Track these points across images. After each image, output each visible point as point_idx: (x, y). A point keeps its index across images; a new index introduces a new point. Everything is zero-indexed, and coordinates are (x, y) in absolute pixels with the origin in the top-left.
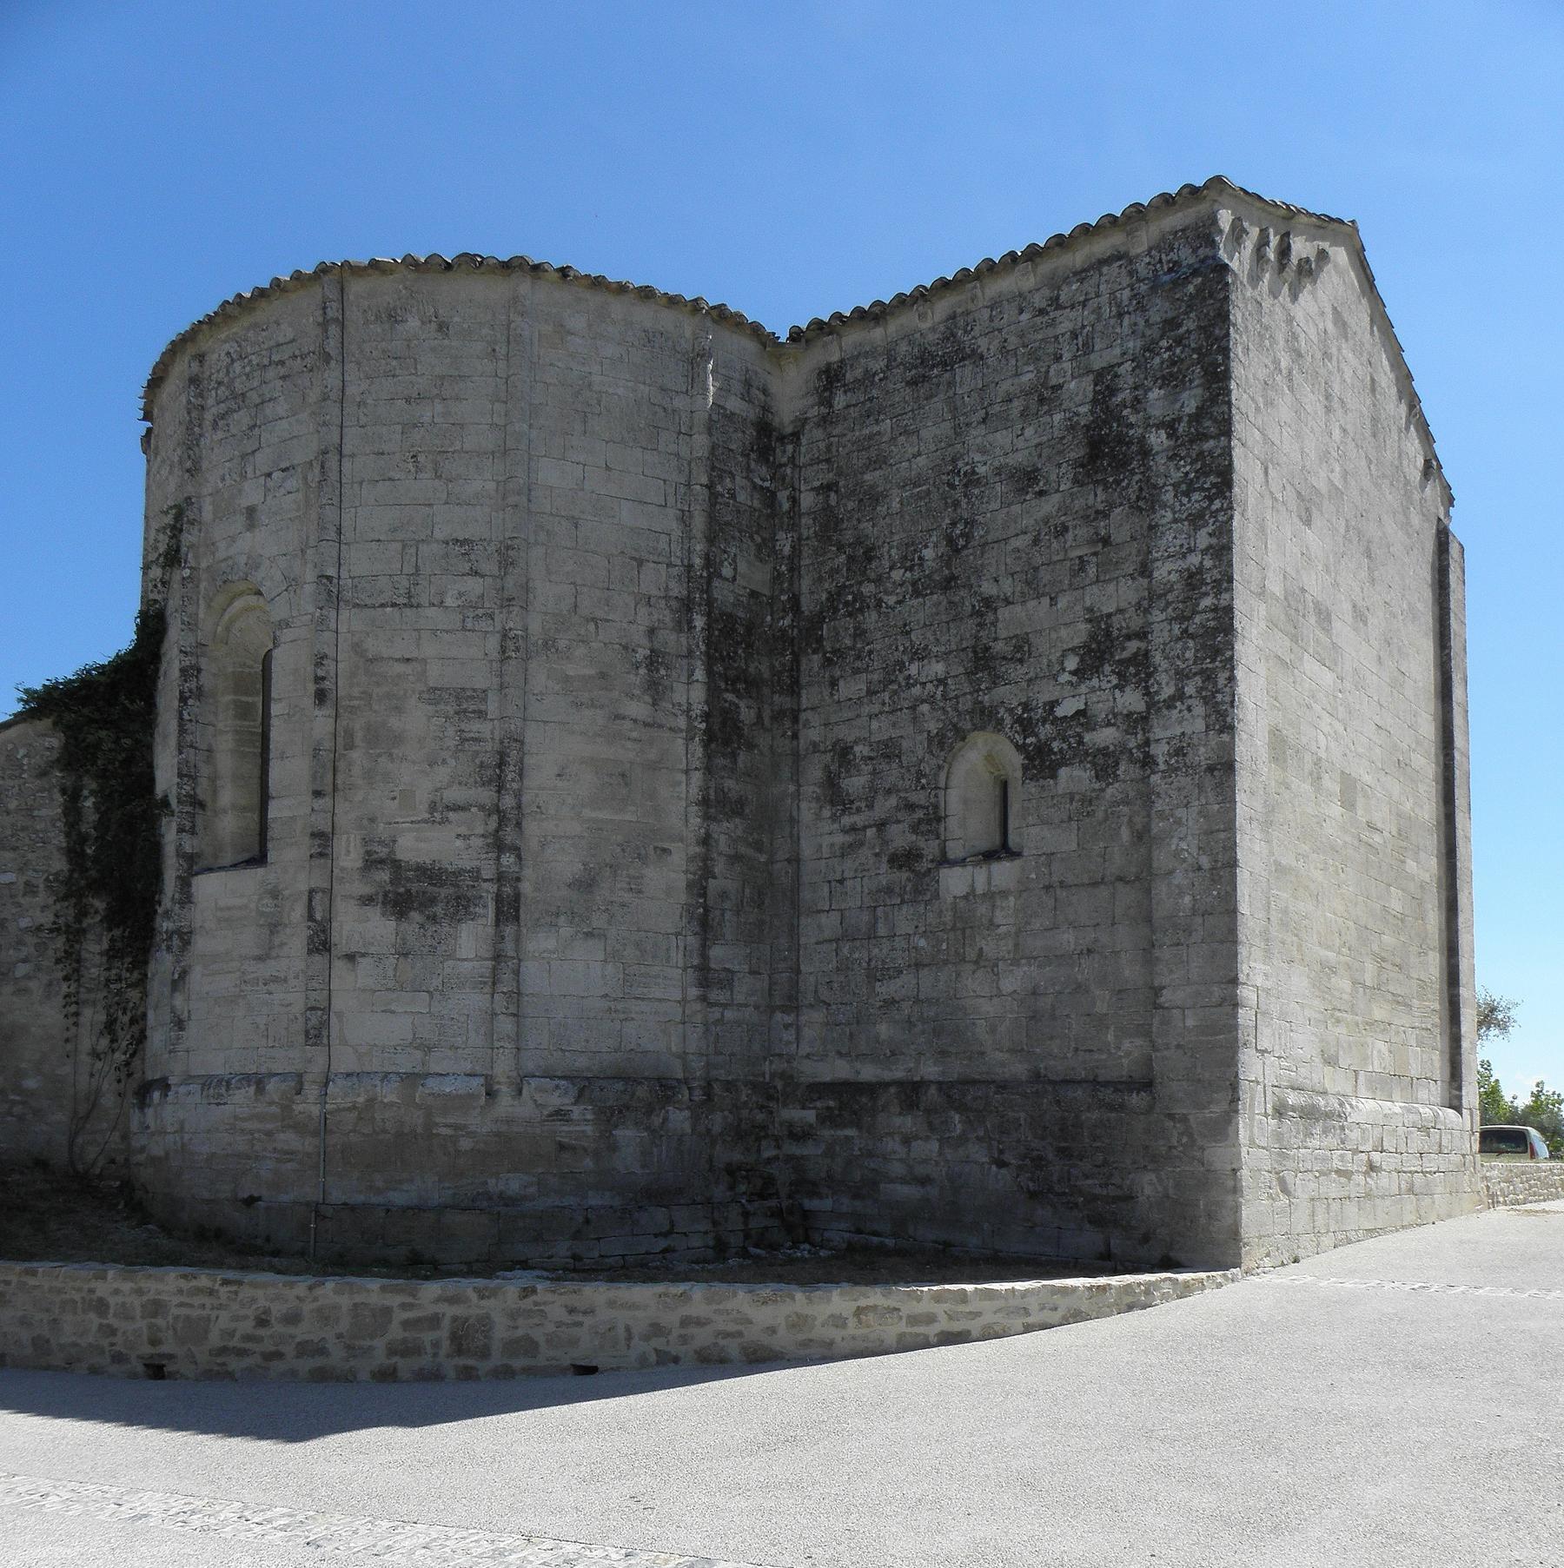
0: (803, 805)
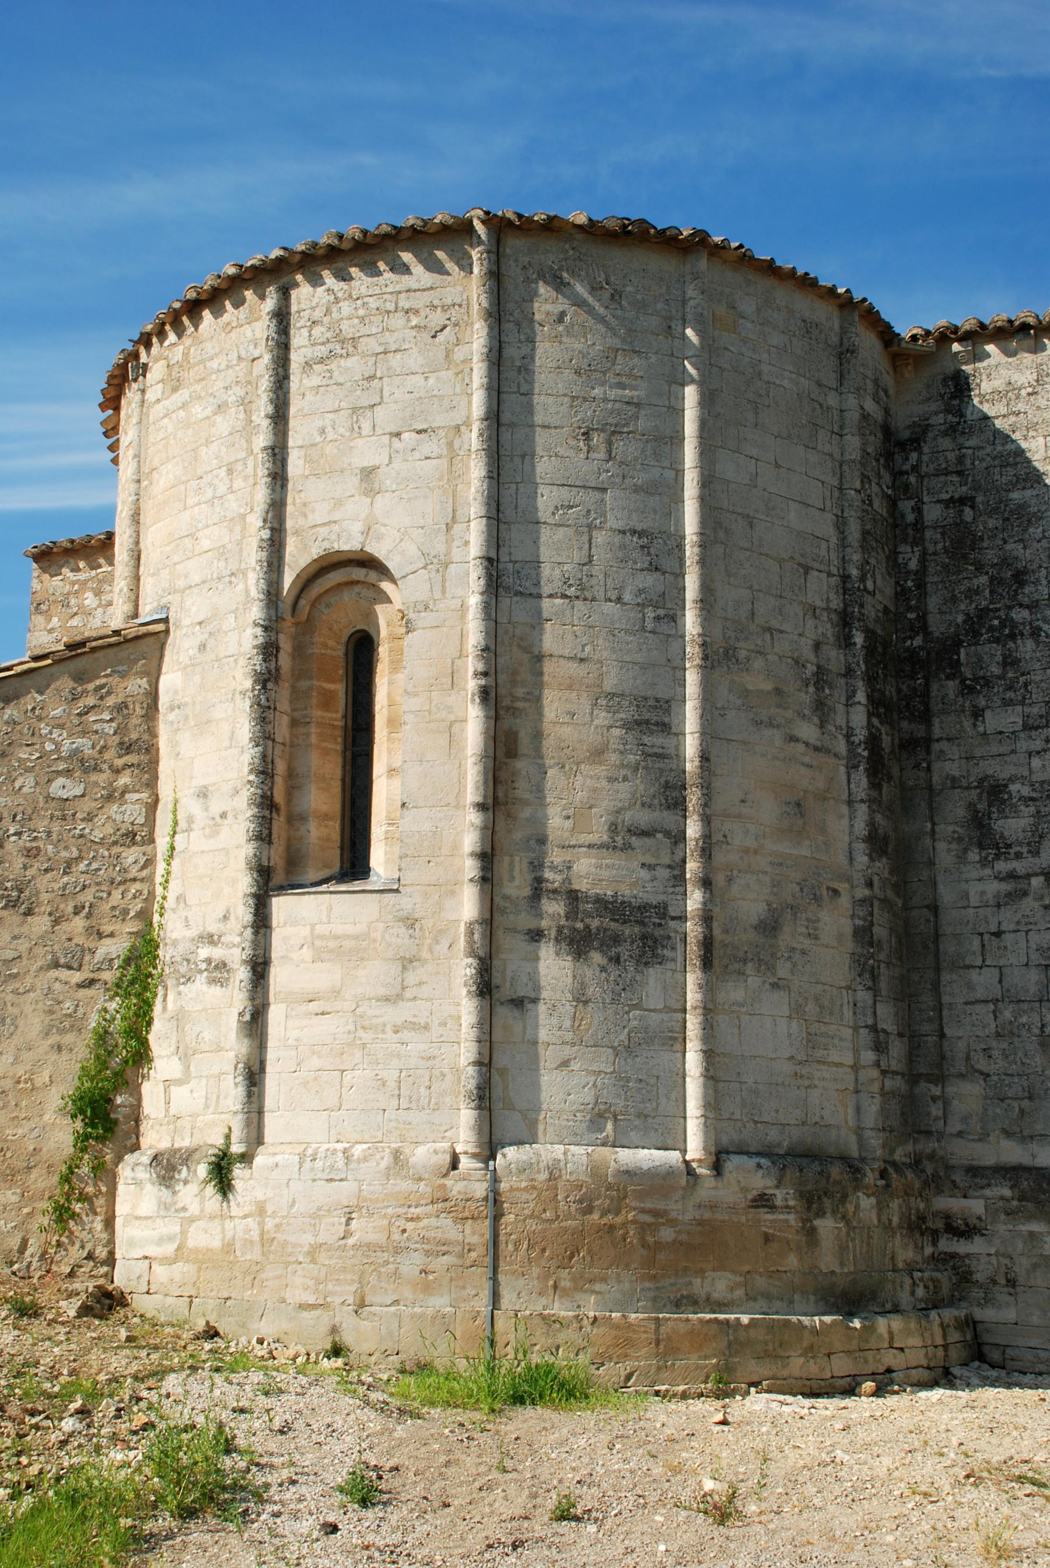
0: (941, 846)
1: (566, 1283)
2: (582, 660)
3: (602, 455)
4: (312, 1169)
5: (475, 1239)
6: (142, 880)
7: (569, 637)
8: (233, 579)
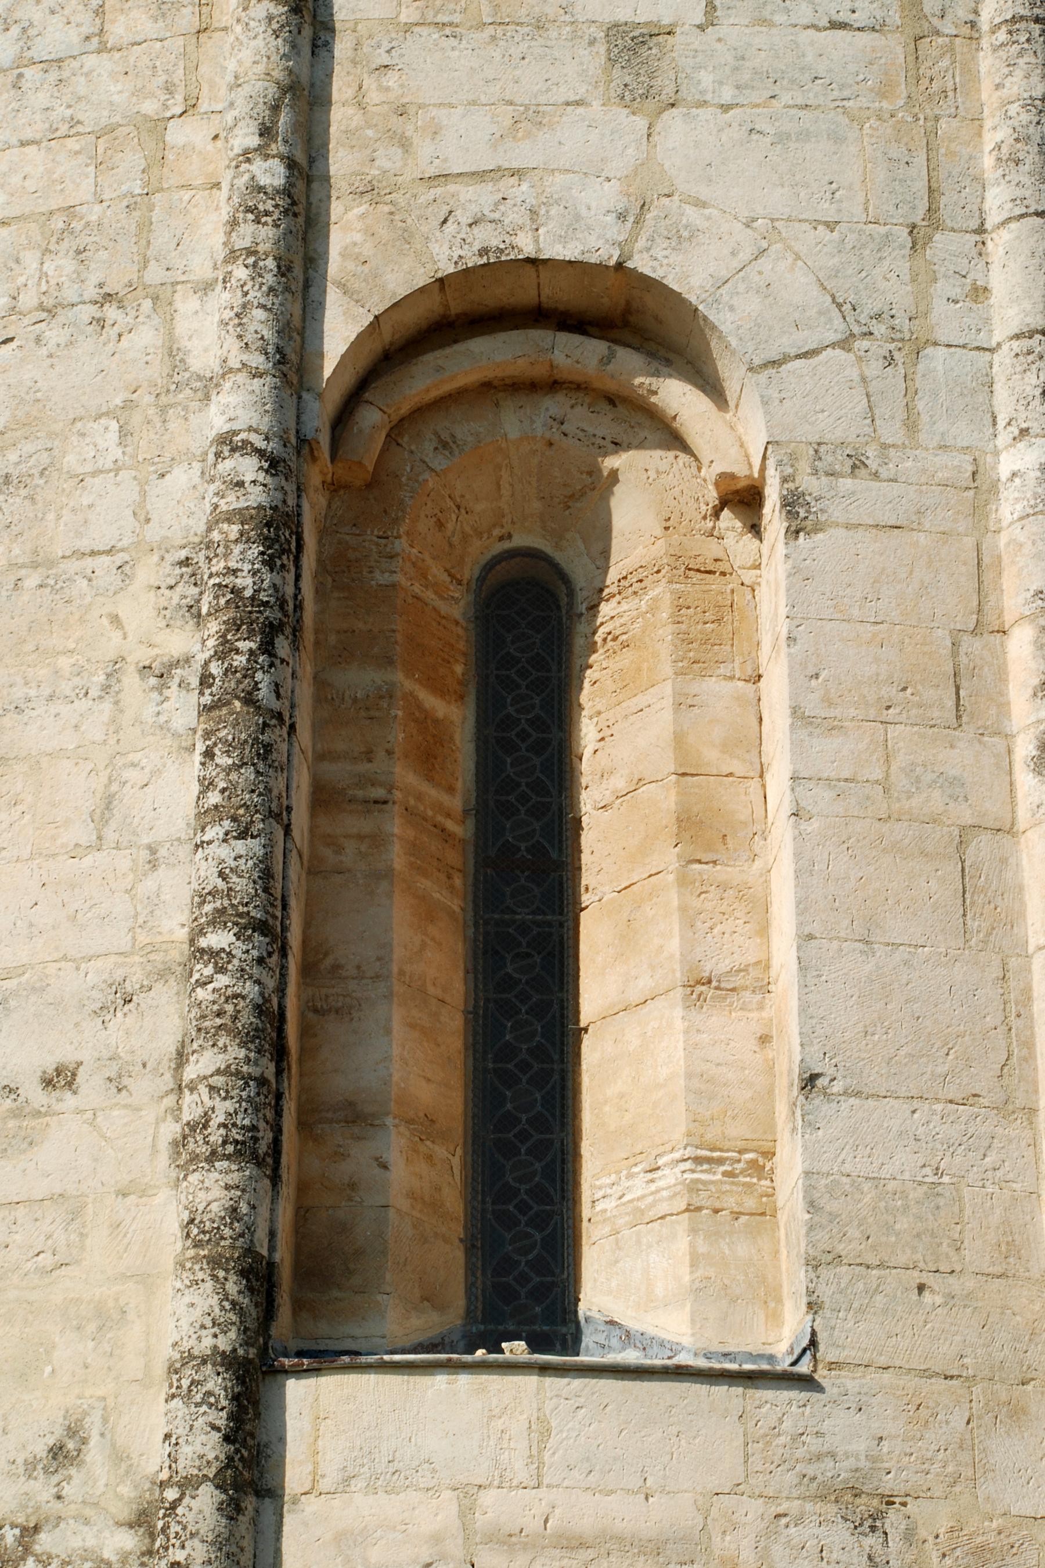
8: (111, 312)
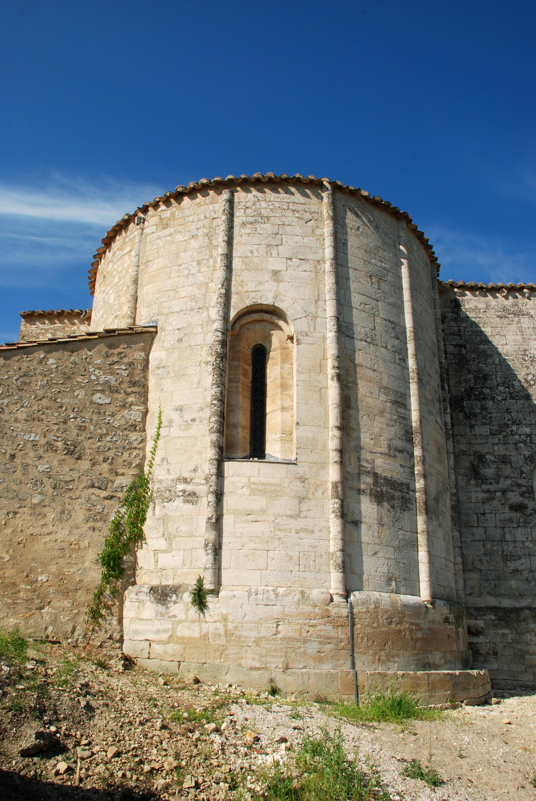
1: (383, 658)
2: (374, 370)
3: (376, 287)
4: (256, 599)
5: (343, 636)
6: (139, 449)
7: (369, 359)
8: (200, 310)
